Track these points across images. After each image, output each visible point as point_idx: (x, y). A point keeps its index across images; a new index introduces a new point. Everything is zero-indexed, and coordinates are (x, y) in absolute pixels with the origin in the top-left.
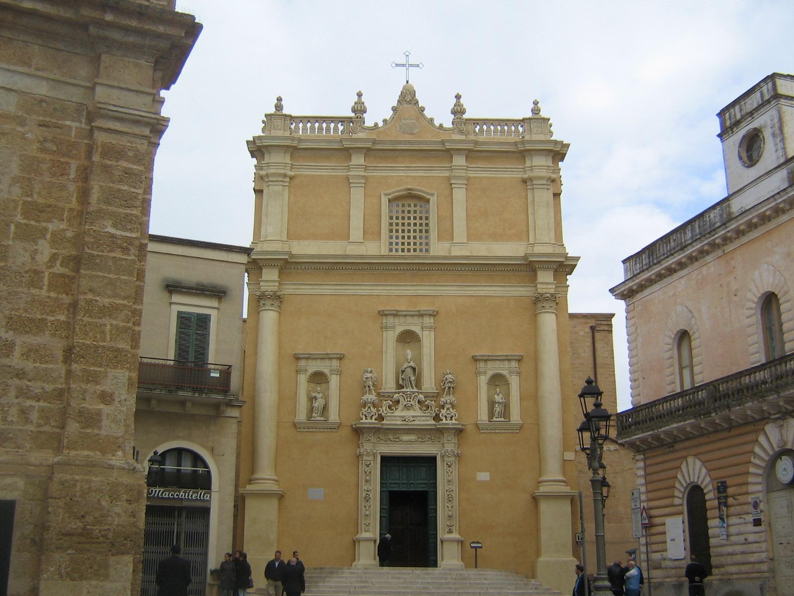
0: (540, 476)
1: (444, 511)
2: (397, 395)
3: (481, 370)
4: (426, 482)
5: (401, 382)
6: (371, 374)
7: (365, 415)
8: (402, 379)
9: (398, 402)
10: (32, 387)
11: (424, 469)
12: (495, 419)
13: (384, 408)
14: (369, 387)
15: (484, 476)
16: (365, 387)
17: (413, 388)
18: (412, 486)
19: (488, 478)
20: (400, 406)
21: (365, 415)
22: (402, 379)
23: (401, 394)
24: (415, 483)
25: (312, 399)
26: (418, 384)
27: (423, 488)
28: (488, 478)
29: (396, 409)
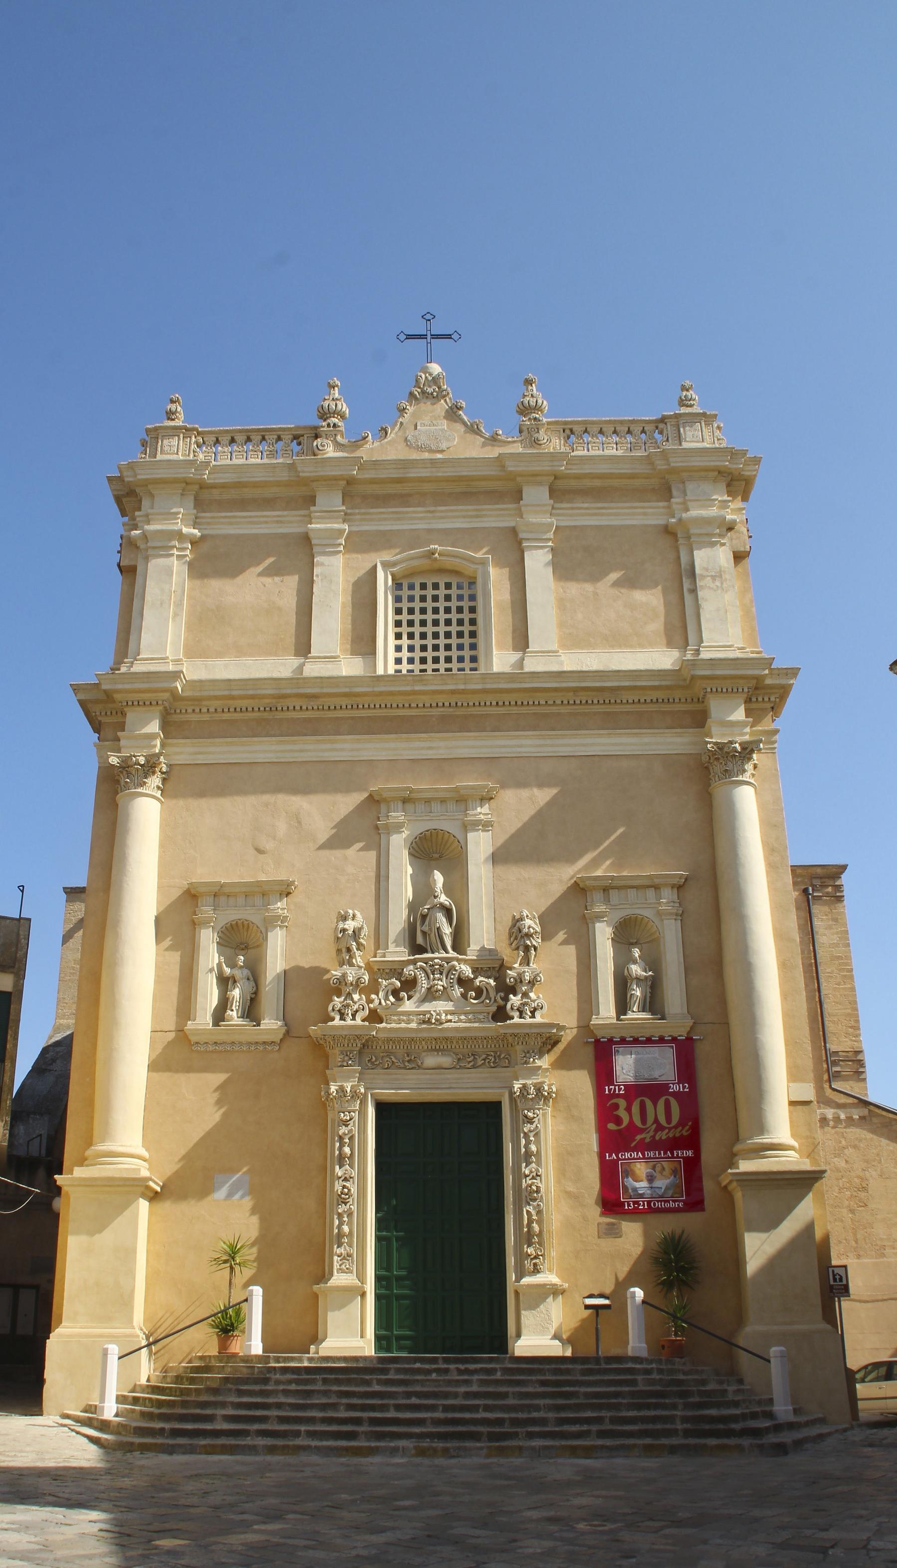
5: (420, 940)
17: (447, 952)
22: (424, 933)
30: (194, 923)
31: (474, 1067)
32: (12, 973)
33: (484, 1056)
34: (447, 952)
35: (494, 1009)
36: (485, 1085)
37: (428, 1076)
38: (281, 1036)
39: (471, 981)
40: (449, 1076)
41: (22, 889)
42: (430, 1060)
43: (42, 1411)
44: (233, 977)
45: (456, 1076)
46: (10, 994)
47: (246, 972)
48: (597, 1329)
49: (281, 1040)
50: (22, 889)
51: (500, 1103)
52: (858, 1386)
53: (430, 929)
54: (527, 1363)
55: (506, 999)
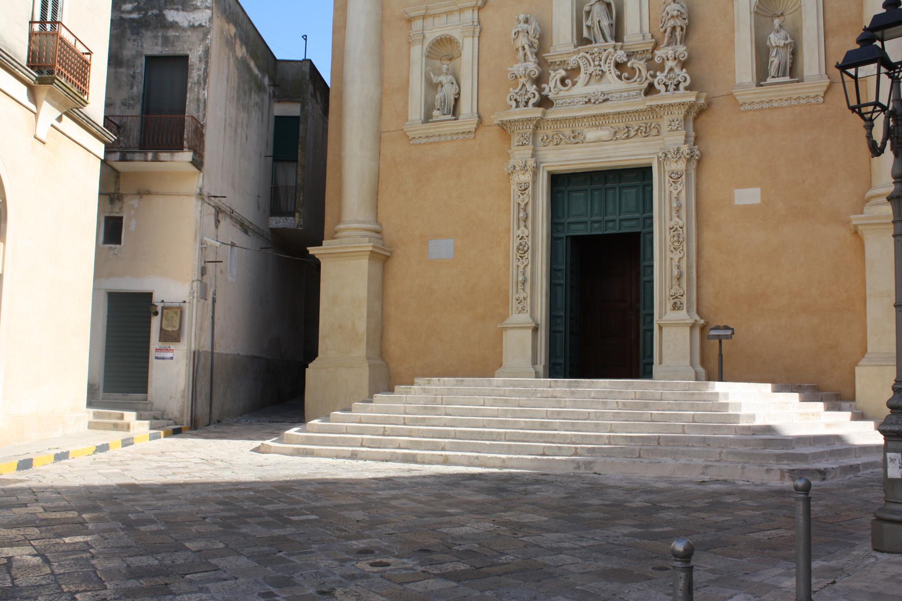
0: (870, 187)
1: (666, 262)
2: (574, 57)
3: (868, 71)
4: (637, 215)
5: (585, 34)
6: (526, 25)
7: (516, 100)
8: (589, 27)
9: (576, 70)
10: (780, 575)
11: (634, 190)
12: (769, 80)
13: (552, 84)
14: (524, 49)
15: (748, 196)
16: (517, 50)
17: (606, 41)
18: (611, 224)
19: (758, 200)
20: (582, 78)
21: (516, 100)
22: (589, 27)
23: (581, 54)
24: (612, 220)
25: (432, 86)
26: (618, 35)
27: (632, 227)
28: (758, 200)
29: (574, 84)
30: (410, 43)
31: (628, 137)
32: (298, 102)
33: (636, 128)
34: (606, 41)
35: (645, 85)
36: (638, 152)
37: (589, 149)
38: (475, 126)
39: (625, 63)
40: (608, 147)
41: (305, 37)
42: (591, 134)
43: (304, 418)
44: (441, 83)
45: (613, 146)
46: (298, 118)
47: (450, 77)
48: (721, 355)
49: (476, 129)
50: (305, 37)
51: (651, 167)
52: (772, 36)
53: (593, 23)
54: (313, 450)
55: (654, 76)
